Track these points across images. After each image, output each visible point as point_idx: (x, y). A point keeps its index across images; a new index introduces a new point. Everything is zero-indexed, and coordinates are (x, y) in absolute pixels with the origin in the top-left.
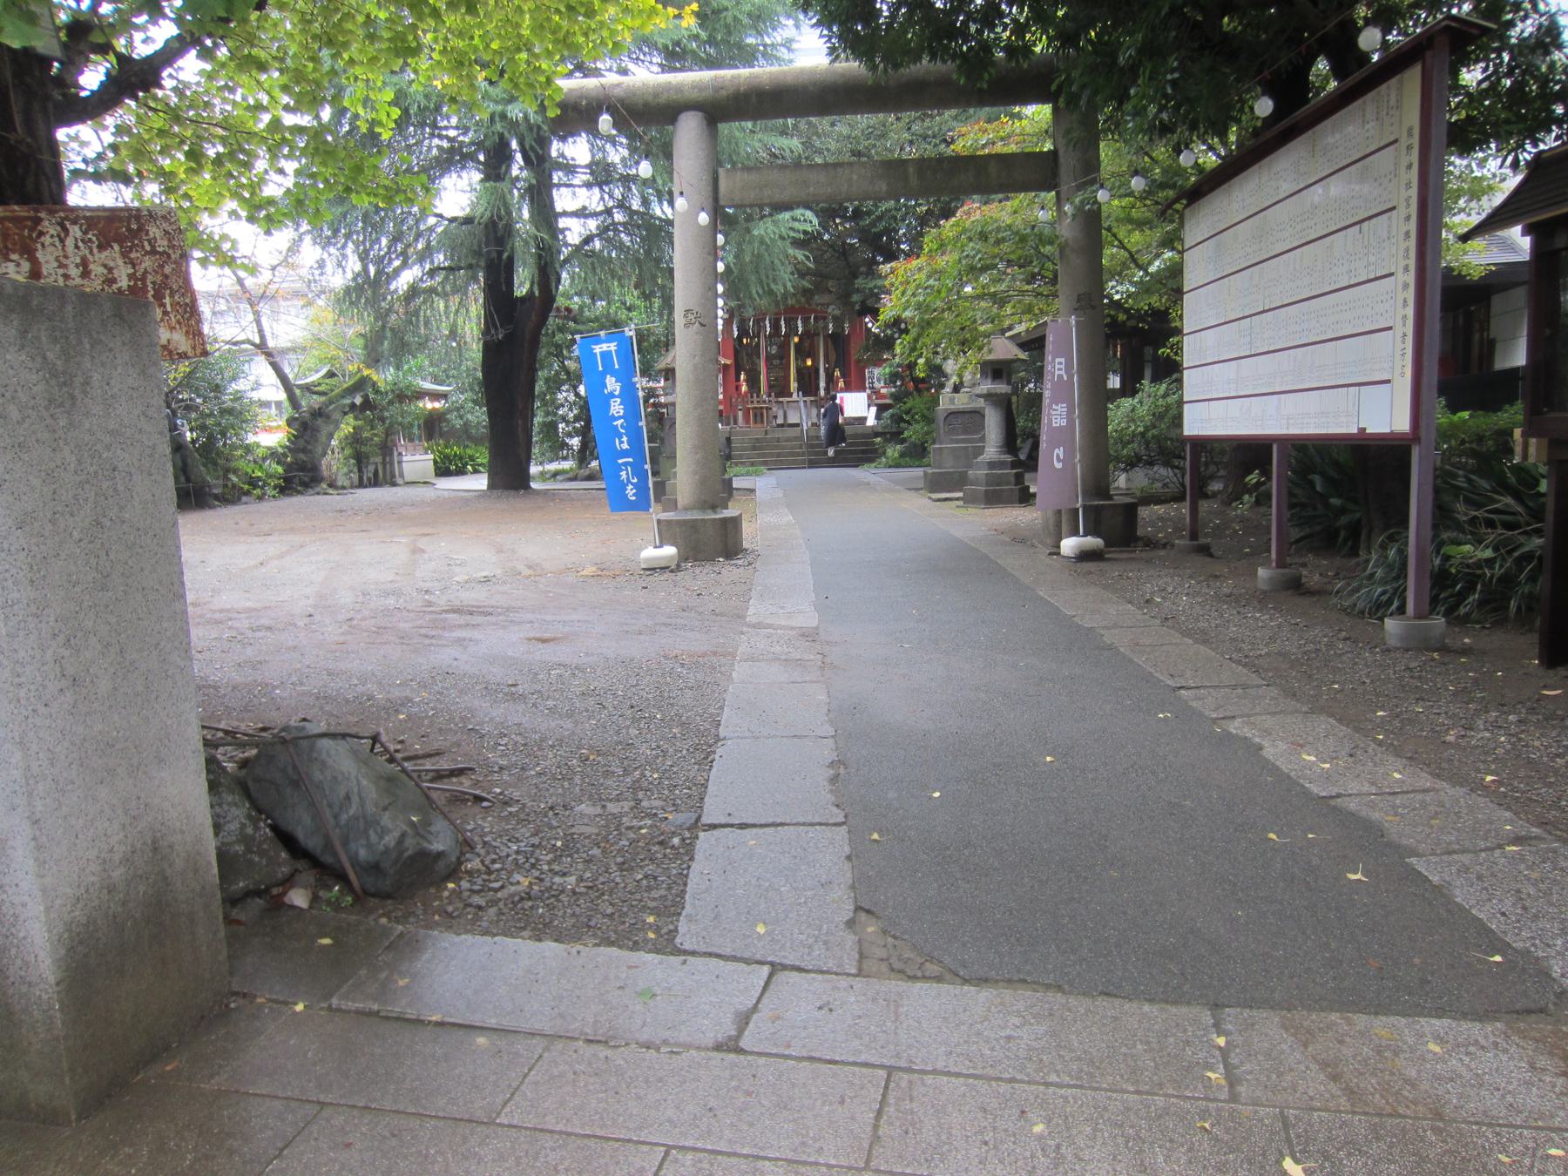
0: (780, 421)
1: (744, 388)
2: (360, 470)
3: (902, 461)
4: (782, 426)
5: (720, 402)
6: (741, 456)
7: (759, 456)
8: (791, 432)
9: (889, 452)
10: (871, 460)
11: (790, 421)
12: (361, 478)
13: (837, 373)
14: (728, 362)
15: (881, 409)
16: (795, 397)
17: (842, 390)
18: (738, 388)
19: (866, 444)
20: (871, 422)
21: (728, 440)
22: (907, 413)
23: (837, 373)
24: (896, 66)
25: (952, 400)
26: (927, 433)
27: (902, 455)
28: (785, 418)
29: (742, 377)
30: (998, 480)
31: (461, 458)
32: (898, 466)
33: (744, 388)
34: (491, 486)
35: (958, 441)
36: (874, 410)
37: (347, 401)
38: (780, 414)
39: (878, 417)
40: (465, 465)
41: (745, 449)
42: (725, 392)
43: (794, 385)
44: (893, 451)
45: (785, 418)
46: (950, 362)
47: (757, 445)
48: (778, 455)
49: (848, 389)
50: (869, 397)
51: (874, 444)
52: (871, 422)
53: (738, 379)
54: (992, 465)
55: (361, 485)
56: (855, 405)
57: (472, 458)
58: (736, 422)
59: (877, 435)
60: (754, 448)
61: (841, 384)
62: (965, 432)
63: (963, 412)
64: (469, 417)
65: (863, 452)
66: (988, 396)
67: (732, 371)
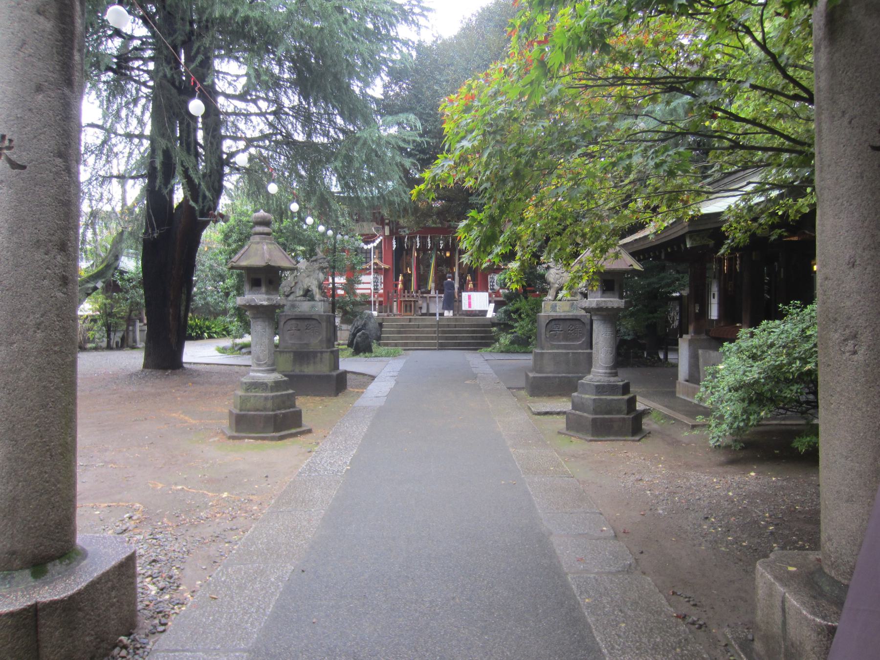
0: (424, 311)
1: (400, 286)
2: (109, 336)
3: (512, 348)
4: (423, 315)
5: (380, 295)
6: (388, 338)
7: (402, 338)
8: (428, 320)
9: (502, 340)
10: (487, 345)
11: (432, 311)
12: (109, 342)
13: (469, 278)
14: (387, 267)
15: (498, 305)
16: (433, 292)
17: (471, 290)
18: (397, 286)
19: (485, 332)
20: (490, 314)
21: (381, 325)
22: (515, 312)
23: (469, 278)
24: (587, 608)
25: (554, 308)
26: (531, 330)
27: (512, 343)
28: (428, 309)
29: (401, 278)
30: (608, 408)
31: (200, 328)
32: (508, 351)
33: (400, 286)
34: (146, 366)
35: (558, 347)
36: (493, 305)
37: (91, 285)
38: (424, 306)
39: (495, 311)
40: (202, 333)
41: (393, 332)
42: (384, 288)
43: (431, 285)
44: (505, 339)
45: (428, 309)
46: (552, 271)
47: (402, 330)
48: (417, 338)
49: (476, 289)
50: (490, 296)
51: (491, 332)
52: (490, 314)
53: (397, 279)
54: (600, 389)
55: (109, 347)
56: (478, 301)
57: (208, 328)
58: (391, 311)
59: (494, 325)
60: (399, 332)
61: (471, 285)
62: (566, 339)
63: (564, 320)
64: (209, 299)
65: (482, 338)
66: (598, 311)
67: (392, 275)
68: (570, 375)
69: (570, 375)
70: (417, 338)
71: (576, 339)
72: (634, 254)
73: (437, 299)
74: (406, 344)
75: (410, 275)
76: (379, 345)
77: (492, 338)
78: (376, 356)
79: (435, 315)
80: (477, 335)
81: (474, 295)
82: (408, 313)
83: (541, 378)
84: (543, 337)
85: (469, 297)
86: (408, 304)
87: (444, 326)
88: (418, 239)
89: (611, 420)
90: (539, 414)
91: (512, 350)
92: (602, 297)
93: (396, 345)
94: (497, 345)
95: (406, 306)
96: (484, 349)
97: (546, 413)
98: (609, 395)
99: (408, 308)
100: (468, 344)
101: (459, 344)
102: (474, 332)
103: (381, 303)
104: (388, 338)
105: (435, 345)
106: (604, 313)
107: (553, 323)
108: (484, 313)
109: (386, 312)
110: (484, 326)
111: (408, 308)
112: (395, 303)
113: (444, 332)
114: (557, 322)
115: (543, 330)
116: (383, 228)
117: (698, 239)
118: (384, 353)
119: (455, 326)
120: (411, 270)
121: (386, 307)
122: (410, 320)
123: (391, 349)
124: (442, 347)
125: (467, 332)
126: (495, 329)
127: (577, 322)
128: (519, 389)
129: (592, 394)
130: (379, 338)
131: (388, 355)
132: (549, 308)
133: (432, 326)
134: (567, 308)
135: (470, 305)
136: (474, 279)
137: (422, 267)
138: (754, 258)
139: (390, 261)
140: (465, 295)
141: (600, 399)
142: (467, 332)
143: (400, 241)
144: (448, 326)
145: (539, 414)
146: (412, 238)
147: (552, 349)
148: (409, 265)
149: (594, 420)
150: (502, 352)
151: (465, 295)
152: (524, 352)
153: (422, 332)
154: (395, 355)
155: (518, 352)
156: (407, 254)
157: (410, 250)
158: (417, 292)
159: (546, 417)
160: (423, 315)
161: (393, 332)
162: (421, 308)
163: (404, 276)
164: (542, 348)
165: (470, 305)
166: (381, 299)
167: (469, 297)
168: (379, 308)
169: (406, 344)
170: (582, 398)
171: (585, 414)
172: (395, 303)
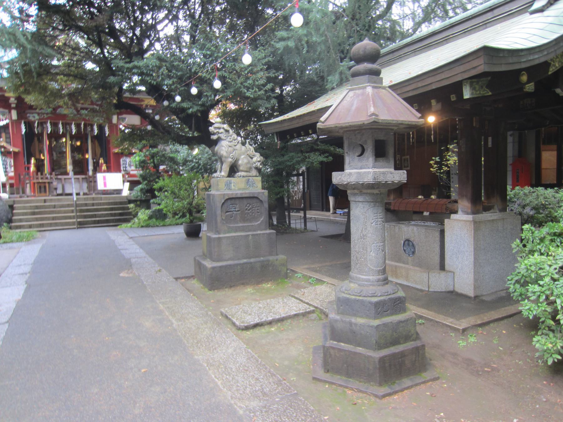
0: (60, 191)
1: (32, 168)
4: (58, 195)
5: (11, 178)
6: (21, 220)
7: (37, 219)
8: (65, 200)
10: (127, 221)
11: (68, 191)
13: (101, 161)
14: (16, 150)
17: (105, 172)
18: (29, 168)
19: (123, 209)
21: (12, 207)
23: (101, 161)
27: (150, 218)
32: (148, 226)
33: (32, 168)
35: (236, 230)
36: (127, 185)
39: (131, 189)
41: (26, 214)
44: (143, 214)
49: (109, 170)
50: (123, 176)
51: (128, 208)
52: (126, 192)
53: (29, 162)
56: (111, 181)
58: (24, 192)
59: (130, 202)
60: (34, 214)
61: (104, 167)
62: (244, 220)
65: (121, 214)
68: (252, 260)
69: (252, 260)
70: (54, 218)
71: (255, 219)
72: (410, 100)
73: (73, 180)
74: (42, 225)
75: (43, 160)
76: (10, 228)
77: (130, 214)
78: (5, 243)
79: (71, 194)
80: (118, 213)
81: (109, 176)
82: (43, 194)
83: (221, 267)
84: (219, 219)
85: (104, 178)
86: (42, 185)
87: (82, 205)
88: (49, 125)
89: (402, 354)
90: (247, 328)
91: (152, 224)
92: (374, 167)
93: (30, 227)
94: (136, 220)
95: (40, 187)
96: (124, 225)
97: (256, 326)
98: (392, 314)
99: (43, 189)
100: (107, 221)
101: (98, 222)
102: (112, 209)
103: (12, 185)
104: (21, 220)
105: (73, 224)
106: (376, 191)
107: (229, 202)
108: (119, 191)
109: (18, 193)
110: (121, 203)
111: (43, 189)
112: (28, 185)
113: (82, 211)
114: (233, 201)
115: (219, 212)
116: (10, 112)
117: (477, 87)
118: (14, 238)
119: (93, 205)
120: (44, 156)
121: (18, 189)
122: (45, 201)
123: (25, 232)
124: (81, 225)
125: (106, 210)
126: (132, 205)
127: (255, 201)
128: (188, 278)
129: (368, 317)
130: (10, 221)
131: (20, 239)
132: (222, 185)
133: (69, 206)
134: (243, 185)
135: (105, 185)
136: (107, 162)
137: (54, 154)
138: (474, 125)
139: (21, 146)
140: (100, 176)
141: (385, 325)
142: (106, 210)
143: (30, 125)
144: (86, 205)
145: (247, 328)
146: (42, 124)
147: (229, 232)
148: (41, 151)
149: (382, 360)
150: (142, 227)
151: (100, 176)
152: (164, 226)
153: (59, 212)
154: (28, 239)
155: (157, 226)
156: (39, 139)
157: (41, 135)
158: (51, 174)
159: (257, 331)
160: (58, 195)
161: (26, 214)
162: (56, 189)
163: (36, 159)
164: (218, 232)
165: (105, 185)
166: (12, 181)
167: (104, 178)
168: (10, 190)
169: (42, 225)
170: (351, 324)
171: (360, 350)
172: (28, 185)
